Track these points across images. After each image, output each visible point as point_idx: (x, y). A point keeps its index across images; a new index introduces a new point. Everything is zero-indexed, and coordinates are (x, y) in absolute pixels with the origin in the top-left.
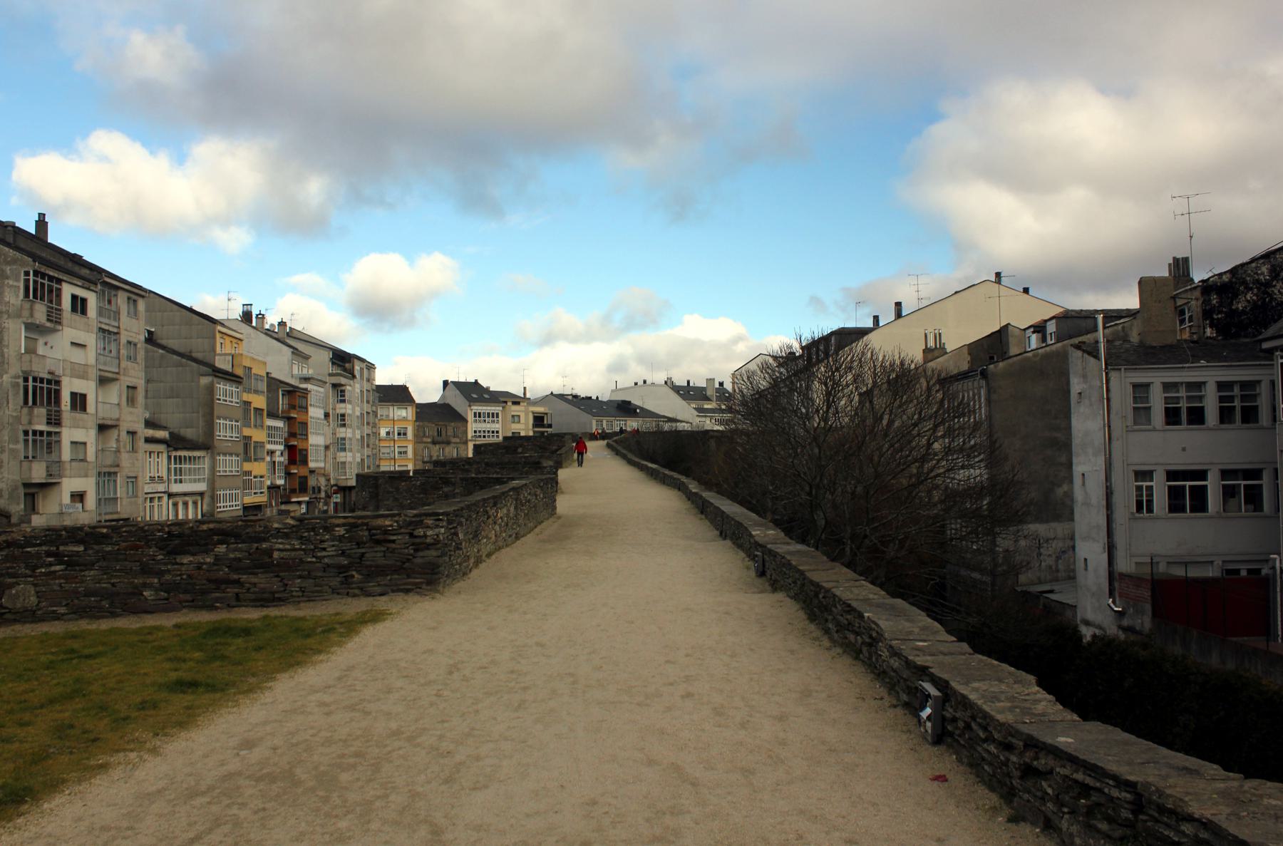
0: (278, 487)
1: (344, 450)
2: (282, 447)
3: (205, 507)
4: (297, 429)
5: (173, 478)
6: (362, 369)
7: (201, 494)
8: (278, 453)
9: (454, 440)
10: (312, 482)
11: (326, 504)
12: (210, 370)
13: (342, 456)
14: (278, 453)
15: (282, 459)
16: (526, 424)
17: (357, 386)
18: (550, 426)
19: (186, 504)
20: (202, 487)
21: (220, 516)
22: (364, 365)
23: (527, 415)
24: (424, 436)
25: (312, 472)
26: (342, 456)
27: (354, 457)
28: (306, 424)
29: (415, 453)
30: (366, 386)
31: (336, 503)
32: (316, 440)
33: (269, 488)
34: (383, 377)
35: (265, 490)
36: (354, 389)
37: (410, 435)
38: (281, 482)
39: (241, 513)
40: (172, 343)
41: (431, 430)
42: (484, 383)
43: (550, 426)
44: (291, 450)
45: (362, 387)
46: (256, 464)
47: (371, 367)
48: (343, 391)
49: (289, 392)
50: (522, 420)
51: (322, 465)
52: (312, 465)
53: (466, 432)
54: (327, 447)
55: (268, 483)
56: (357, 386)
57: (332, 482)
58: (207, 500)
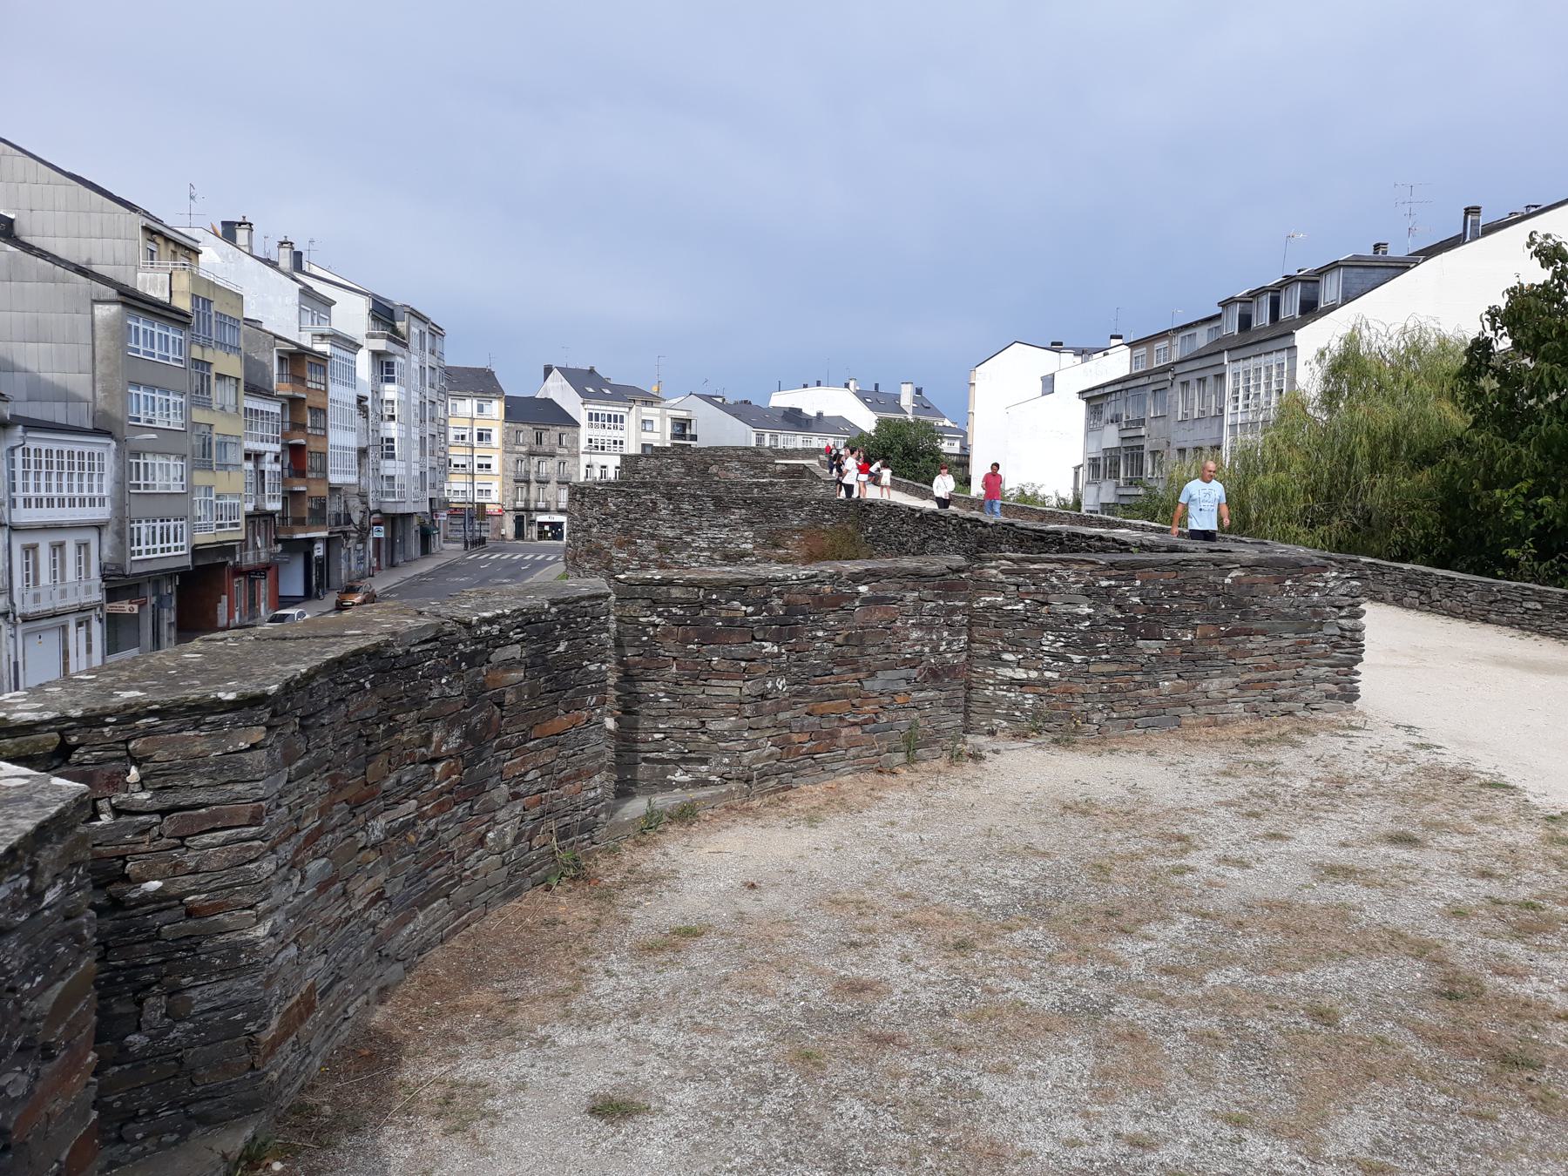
0: (272, 514)
1: (392, 456)
2: (278, 448)
3: (106, 552)
4: (302, 414)
5: (19, 494)
6: (422, 334)
7: (99, 527)
8: (269, 457)
9: (559, 451)
10: (333, 507)
11: (362, 540)
12: (111, 293)
13: (388, 467)
14: (269, 457)
15: (278, 467)
16: (662, 432)
17: (415, 358)
18: (694, 438)
19: (58, 547)
20: (102, 513)
21: (138, 569)
22: (424, 328)
23: (663, 420)
24: (517, 443)
25: (335, 489)
26: (388, 467)
27: (409, 468)
28: (324, 411)
29: (504, 469)
30: (429, 360)
31: (378, 541)
32: (342, 438)
33: (248, 516)
34: (457, 356)
35: (242, 520)
36: (409, 362)
37: (496, 468)
38: (275, 506)
39: (188, 562)
40: (59, 248)
41: (527, 433)
42: (601, 371)
43: (694, 438)
44: (296, 452)
45: (423, 361)
46: (222, 474)
47: (437, 332)
48: (390, 364)
49: (291, 354)
50: (657, 427)
51: (353, 479)
52: (334, 479)
53: (576, 441)
54: (363, 452)
55: (250, 507)
56: (415, 358)
57: (372, 506)
58: (109, 538)
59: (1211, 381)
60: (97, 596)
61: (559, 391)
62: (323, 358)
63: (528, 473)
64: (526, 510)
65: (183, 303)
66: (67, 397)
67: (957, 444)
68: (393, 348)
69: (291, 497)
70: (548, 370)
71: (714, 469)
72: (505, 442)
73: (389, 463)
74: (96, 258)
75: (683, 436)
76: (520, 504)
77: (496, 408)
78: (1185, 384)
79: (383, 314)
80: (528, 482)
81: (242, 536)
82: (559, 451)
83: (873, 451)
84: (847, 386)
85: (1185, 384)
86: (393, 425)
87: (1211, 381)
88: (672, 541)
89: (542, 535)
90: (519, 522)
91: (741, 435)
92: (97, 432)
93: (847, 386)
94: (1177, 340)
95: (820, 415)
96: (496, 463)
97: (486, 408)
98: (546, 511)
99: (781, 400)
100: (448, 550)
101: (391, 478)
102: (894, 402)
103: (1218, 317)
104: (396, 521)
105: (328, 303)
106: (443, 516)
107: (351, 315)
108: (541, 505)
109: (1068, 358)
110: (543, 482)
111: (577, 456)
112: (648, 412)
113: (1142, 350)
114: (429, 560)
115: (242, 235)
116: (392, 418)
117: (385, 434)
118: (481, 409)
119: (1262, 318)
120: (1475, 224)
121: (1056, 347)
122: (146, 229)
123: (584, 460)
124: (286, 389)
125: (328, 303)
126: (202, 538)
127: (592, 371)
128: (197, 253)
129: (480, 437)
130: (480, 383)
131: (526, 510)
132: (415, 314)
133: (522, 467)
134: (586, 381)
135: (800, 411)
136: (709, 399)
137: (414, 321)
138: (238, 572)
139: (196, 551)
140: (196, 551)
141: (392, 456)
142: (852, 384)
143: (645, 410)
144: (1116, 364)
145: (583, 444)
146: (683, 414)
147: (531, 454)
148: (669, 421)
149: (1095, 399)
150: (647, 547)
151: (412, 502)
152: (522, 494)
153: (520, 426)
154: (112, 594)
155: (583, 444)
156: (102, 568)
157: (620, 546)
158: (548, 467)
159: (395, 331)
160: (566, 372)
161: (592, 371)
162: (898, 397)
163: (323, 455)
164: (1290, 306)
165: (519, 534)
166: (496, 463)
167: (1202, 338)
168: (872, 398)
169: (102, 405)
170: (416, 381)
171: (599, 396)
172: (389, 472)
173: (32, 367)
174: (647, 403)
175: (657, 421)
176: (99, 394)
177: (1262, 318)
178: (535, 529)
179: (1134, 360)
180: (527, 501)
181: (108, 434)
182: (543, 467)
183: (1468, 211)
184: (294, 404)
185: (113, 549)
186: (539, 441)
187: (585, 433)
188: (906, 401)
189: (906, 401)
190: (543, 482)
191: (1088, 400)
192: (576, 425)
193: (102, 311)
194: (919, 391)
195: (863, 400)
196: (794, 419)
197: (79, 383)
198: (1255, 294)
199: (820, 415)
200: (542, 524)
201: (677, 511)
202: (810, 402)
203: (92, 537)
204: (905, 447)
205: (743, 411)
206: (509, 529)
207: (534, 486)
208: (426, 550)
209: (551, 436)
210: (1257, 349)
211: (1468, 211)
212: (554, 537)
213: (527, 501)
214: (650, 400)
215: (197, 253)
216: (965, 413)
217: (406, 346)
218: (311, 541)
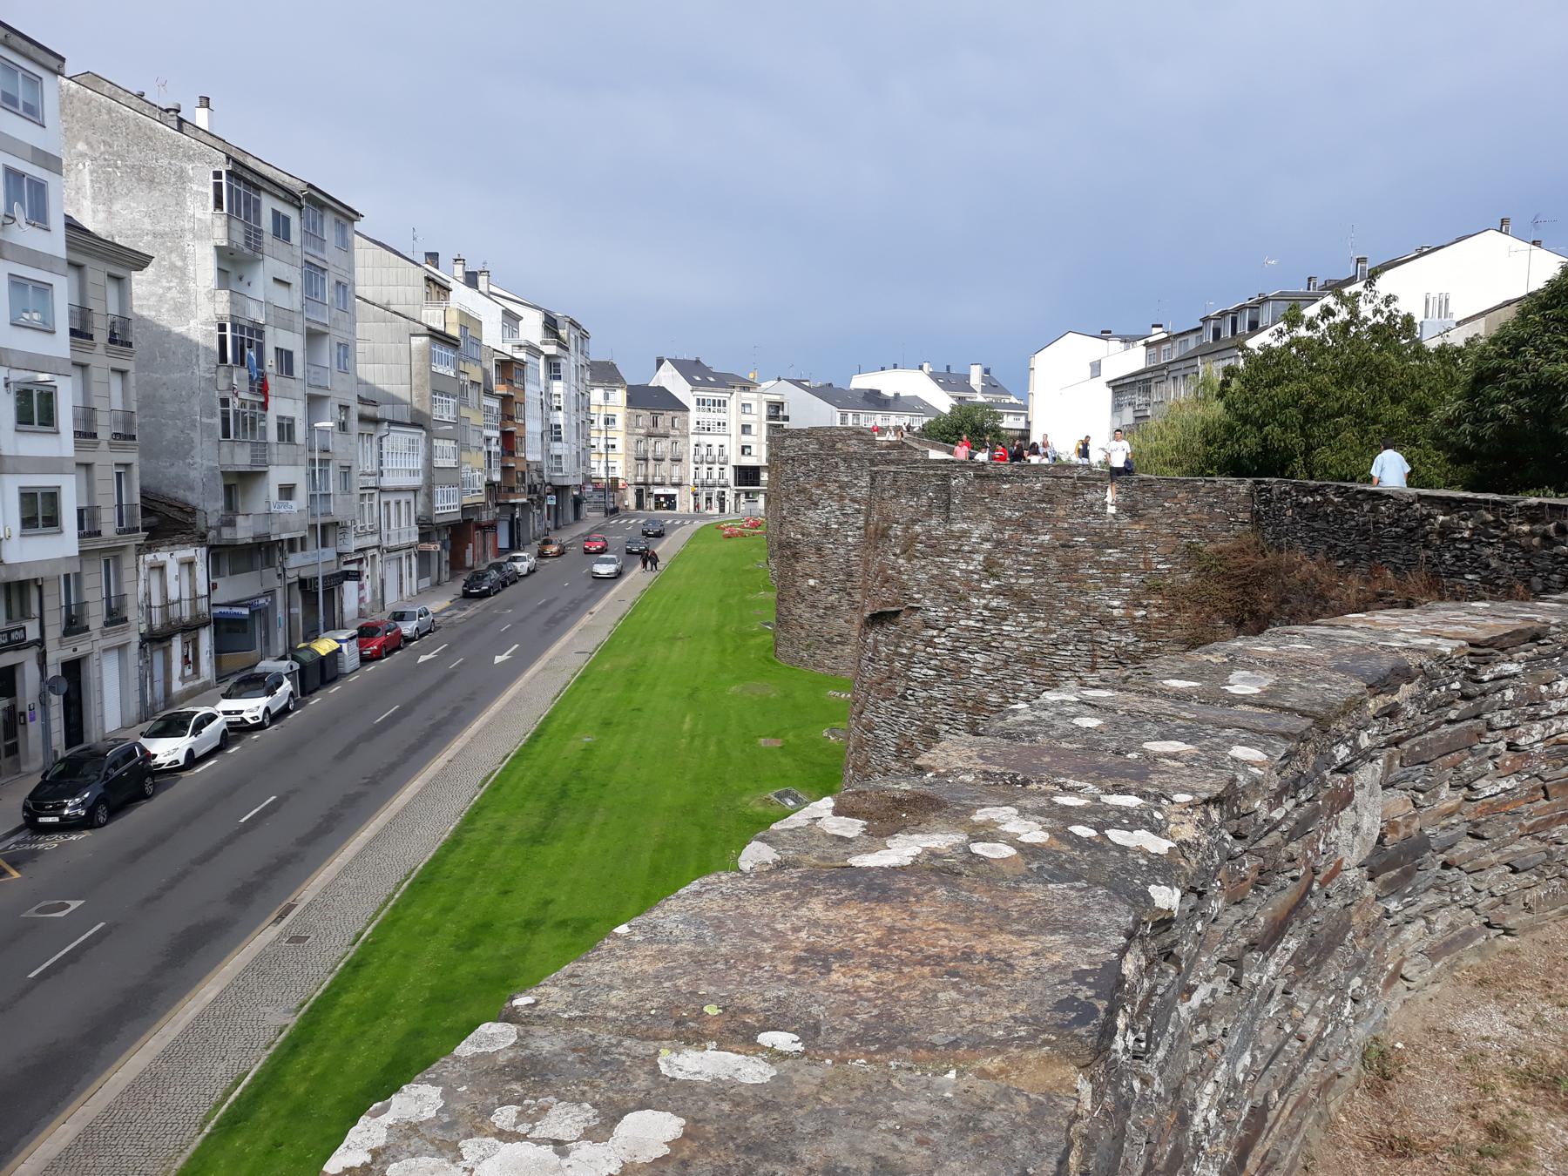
1: (559, 439)
2: (497, 434)
3: (419, 508)
7: (415, 491)
8: (494, 441)
11: (540, 507)
13: (557, 448)
14: (494, 441)
18: (786, 418)
20: (417, 481)
22: (578, 333)
23: (759, 403)
24: (637, 426)
29: (627, 449)
30: (581, 361)
32: (533, 426)
41: (645, 417)
42: (706, 362)
43: (786, 418)
50: (754, 410)
53: (687, 424)
58: (421, 498)
59: (1180, 379)
60: (416, 539)
61: (670, 380)
62: (522, 364)
63: (646, 451)
64: (646, 484)
65: (454, 331)
66: (394, 400)
67: (1023, 419)
68: (561, 352)
69: (506, 470)
70: (660, 362)
71: (839, 445)
72: (627, 426)
73: (557, 444)
74: (394, 300)
75: (776, 418)
76: (640, 479)
77: (620, 396)
78: (1175, 378)
79: (551, 325)
80: (646, 460)
81: (483, 500)
82: (672, 432)
83: (946, 431)
84: (921, 368)
85: (1175, 378)
86: (560, 414)
87: (1180, 379)
88: (847, 483)
89: (658, 506)
90: (639, 494)
91: (824, 415)
92: (413, 425)
93: (921, 368)
94: (1177, 343)
95: (897, 395)
96: (620, 444)
97: (611, 396)
98: (661, 484)
99: (861, 382)
100: (593, 517)
101: (559, 457)
102: (963, 383)
103: (1200, 329)
104: (560, 490)
105: (518, 318)
106: (589, 488)
107: (532, 327)
108: (658, 479)
109: (1115, 345)
110: (659, 460)
111: (687, 436)
112: (747, 396)
113: (1154, 350)
114: (581, 524)
115: (482, 280)
116: (559, 408)
117: (554, 422)
118: (607, 397)
119: (1227, 333)
120: (1363, 269)
121: (1105, 335)
122: (428, 279)
123: (693, 440)
124: (501, 389)
125: (518, 318)
126: (467, 500)
127: (698, 362)
128: (449, 290)
129: (607, 422)
130: (605, 374)
131: (646, 484)
132: (573, 323)
133: (642, 446)
134: (692, 370)
135: (878, 392)
136: (797, 383)
137: (573, 329)
138: (479, 527)
139: (464, 509)
140: (464, 509)
141: (559, 439)
142: (926, 366)
143: (744, 394)
144: (1134, 359)
145: (692, 426)
146: (777, 398)
147: (650, 435)
148: (765, 405)
149: (1119, 387)
150: (833, 487)
151: (569, 475)
152: (642, 470)
153: (640, 412)
154: (425, 537)
155: (692, 426)
156: (418, 520)
157: (818, 487)
158: (663, 446)
159: (558, 337)
160: (674, 362)
161: (698, 362)
162: (968, 377)
163: (523, 438)
164: (1243, 327)
165: (640, 505)
166: (620, 444)
167: (1192, 343)
168: (949, 380)
169: (417, 405)
170: (573, 377)
171: (705, 384)
172: (557, 452)
173: (370, 380)
174: (745, 389)
175: (754, 404)
176: (415, 399)
177: (1227, 333)
178: (652, 500)
179: (1148, 356)
180: (646, 476)
181: (420, 426)
182: (659, 446)
183: (1358, 261)
184: (506, 400)
185: (424, 506)
186: (655, 424)
187: (694, 415)
188: (976, 379)
189: (976, 379)
190: (659, 460)
191: (1114, 388)
192: (686, 409)
193: (418, 342)
194: (987, 371)
195: (936, 380)
196: (874, 400)
197: (401, 391)
198: (1223, 314)
199: (897, 395)
200: (657, 497)
201: (849, 467)
202: (888, 383)
203: (411, 497)
204: (973, 425)
205: (827, 393)
206: (631, 501)
207: (651, 463)
208: (577, 517)
209: (665, 420)
210: (1217, 356)
211: (1358, 261)
212: (668, 508)
213: (646, 476)
214: (747, 387)
215: (449, 290)
216: (1025, 394)
217: (567, 349)
218: (514, 505)
